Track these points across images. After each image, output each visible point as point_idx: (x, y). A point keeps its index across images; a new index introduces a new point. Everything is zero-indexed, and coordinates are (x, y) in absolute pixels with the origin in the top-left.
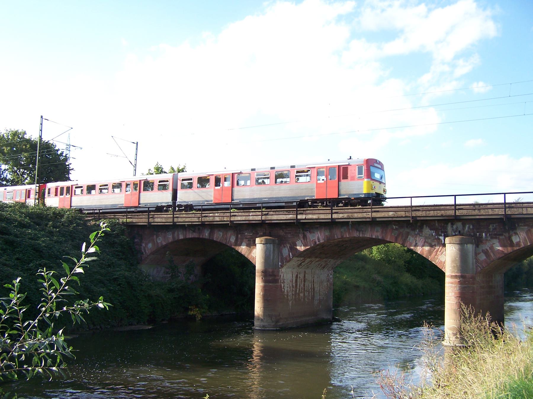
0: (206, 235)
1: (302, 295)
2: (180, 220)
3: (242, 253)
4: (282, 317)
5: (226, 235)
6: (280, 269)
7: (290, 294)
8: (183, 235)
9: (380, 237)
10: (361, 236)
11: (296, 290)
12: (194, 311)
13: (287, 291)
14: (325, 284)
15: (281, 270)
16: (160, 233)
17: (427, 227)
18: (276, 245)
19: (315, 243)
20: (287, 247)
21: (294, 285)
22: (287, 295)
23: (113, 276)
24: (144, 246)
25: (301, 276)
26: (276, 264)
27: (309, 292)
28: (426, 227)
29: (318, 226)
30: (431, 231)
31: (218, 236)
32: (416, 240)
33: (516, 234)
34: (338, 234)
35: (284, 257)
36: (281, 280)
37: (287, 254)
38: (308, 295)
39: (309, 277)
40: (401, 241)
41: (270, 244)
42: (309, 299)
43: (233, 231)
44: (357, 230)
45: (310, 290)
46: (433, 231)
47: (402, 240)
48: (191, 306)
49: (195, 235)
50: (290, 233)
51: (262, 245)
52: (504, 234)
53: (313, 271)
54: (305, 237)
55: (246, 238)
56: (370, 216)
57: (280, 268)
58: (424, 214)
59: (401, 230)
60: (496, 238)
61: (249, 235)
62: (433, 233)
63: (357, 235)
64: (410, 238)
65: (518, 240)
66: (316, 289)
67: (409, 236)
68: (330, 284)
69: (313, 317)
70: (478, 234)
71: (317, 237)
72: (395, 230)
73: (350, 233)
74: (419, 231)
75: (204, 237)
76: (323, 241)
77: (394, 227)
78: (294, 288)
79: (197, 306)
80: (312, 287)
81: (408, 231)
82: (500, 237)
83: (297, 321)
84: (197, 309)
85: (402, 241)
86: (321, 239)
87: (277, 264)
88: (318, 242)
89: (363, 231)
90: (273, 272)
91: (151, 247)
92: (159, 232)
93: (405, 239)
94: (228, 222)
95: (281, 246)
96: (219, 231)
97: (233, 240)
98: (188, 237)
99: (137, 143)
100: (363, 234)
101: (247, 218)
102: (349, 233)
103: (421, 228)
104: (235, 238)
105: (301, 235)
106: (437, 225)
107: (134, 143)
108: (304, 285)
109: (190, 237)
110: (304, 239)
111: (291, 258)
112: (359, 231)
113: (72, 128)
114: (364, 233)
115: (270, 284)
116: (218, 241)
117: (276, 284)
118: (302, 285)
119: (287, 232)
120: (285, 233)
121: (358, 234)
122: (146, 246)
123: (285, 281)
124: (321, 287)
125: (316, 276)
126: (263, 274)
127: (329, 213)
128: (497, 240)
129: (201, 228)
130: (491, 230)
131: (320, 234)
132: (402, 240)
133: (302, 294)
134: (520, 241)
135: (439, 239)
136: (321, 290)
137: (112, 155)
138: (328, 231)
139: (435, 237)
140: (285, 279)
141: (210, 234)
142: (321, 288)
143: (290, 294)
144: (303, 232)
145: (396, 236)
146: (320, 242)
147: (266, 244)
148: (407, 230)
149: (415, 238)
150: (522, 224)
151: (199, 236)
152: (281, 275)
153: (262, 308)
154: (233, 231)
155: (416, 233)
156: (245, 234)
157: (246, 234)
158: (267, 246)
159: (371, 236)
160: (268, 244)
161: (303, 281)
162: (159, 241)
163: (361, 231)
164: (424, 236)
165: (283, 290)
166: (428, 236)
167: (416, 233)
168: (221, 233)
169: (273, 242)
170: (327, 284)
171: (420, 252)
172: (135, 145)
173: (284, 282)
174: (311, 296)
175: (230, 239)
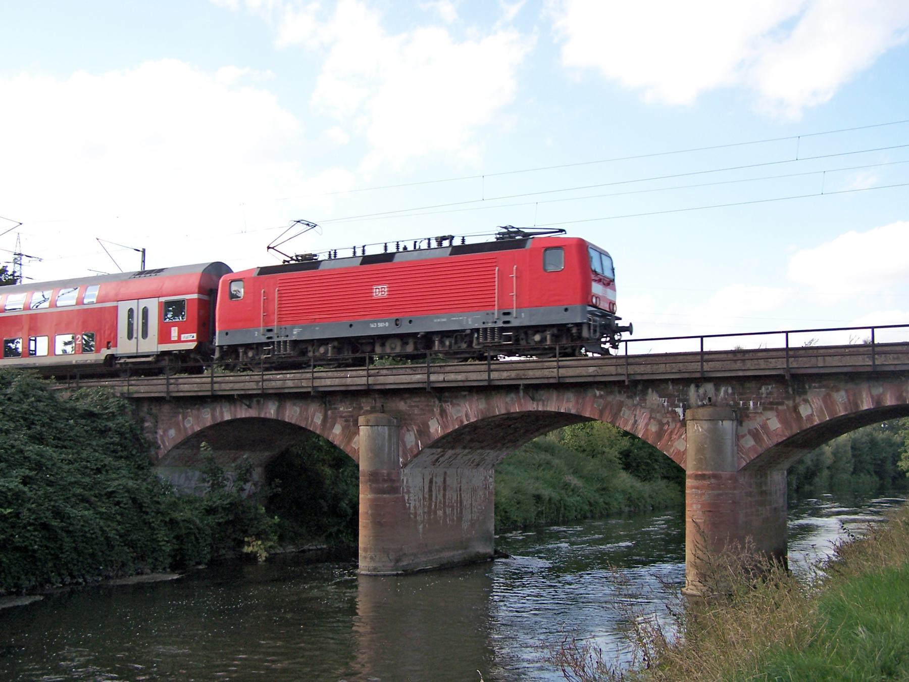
0: (270, 413)
1: (440, 513)
6: (402, 470)
7: (420, 511)
8: (231, 413)
11: (430, 505)
12: (253, 546)
13: (415, 507)
14: (481, 493)
19: (462, 422)
21: (427, 496)
22: (415, 514)
24: (162, 434)
25: (439, 480)
27: (452, 507)
28: (653, 391)
31: (292, 414)
33: (806, 401)
35: (408, 447)
36: (403, 488)
37: (414, 443)
39: (452, 481)
43: (318, 404)
44: (533, 399)
45: (455, 504)
50: (418, 406)
52: (787, 402)
54: (443, 413)
55: (341, 417)
56: (555, 374)
60: (772, 409)
65: (809, 412)
67: (623, 409)
68: (489, 492)
70: (741, 402)
72: (598, 397)
73: (521, 405)
74: (640, 400)
75: (268, 416)
77: (598, 393)
79: (258, 536)
81: (622, 399)
82: (780, 407)
84: (260, 542)
89: (543, 401)
90: (389, 474)
93: (616, 414)
94: (309, 390)
95: (402, 429)
96: (294, 404)
99: (144, 251)
100: (543, 405)
101: (343, 381)
103: (644, 393)
104: (321, 418)
108: (444, 496)
112: (538, 401)
113: (21, 224)
115: (385, 496)
118: (440, 497)
120: (409, 407)
125: (464, 481)
128: (775, 413)
130: (764, 396)
134: (812, 415)
135: (675, 412)
136: (473, 505)
141: (278, 411)
145: (601, 408)
150: (817, 385)
154: (318, 404)
157: (341, 409)
161: (442, 488)
162: (188, 425)
165: (408, 505)
168: (298, 409)
170: (485, 494)
173: (408, 492)
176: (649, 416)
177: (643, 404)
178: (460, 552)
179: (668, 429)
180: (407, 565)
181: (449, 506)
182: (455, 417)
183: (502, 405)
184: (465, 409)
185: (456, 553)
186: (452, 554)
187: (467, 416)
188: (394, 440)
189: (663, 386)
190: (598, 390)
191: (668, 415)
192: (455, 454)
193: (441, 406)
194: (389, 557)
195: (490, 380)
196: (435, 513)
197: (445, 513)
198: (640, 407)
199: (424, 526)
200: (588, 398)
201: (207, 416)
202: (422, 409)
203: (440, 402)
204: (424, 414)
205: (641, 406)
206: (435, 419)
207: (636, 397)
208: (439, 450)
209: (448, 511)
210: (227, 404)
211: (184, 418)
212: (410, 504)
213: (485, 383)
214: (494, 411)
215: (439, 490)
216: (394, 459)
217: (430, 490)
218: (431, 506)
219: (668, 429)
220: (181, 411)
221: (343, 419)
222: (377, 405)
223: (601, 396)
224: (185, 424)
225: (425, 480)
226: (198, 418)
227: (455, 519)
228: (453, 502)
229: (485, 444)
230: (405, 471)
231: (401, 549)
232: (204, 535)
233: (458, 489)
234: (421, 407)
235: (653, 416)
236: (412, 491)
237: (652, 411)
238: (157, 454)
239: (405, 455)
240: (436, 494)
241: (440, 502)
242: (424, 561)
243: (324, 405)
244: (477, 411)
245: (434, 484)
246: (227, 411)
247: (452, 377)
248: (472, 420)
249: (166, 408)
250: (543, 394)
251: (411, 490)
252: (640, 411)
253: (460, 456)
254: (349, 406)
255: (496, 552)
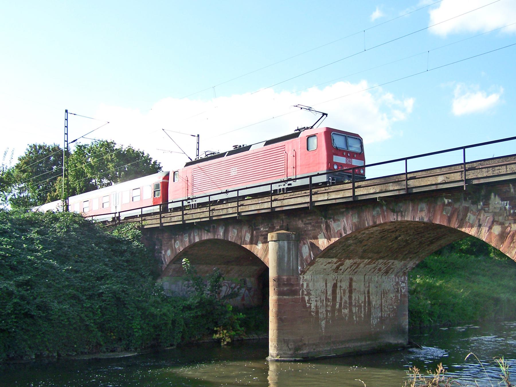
1: (346, 311)
2: (190, 217)
3: (258, 256)
4: (307, 343)
5: (241, 233)
6: (301, 276)
7: (322, 310)
8: (199, 236)
9: (426, 220)
10: (399, 219)
11: (334, 305)
12: (220, 333)
13: (316, 306)
14: (392, 295)
15: (303, 277)
16: (177, 236)
17: (497, 197)
18: (292, 242)
20: (308, 244)
21: (330, 297)
22: (317, 312)
23: (98, 290)
24: (164, 253)
25: (345, 285)
26: (293, 269)
27: (360, 307)
28: (495, 196)
29: (344, 210)
30: (503, 202)
32: (479, 220)
34: (369, 220)
36: (303, 292)
37: (308, 254)
38: (358, 311)
39: (359, 285)
40: (457, 223)
41: (284, 240)
42: (361, 317)
43: (248, 226)
44: (393, 211)
45: (363, 305)
46: (506, 202)
47: (457, 221)
48: (217, 328)
49: (206, 236)
50: (310, 223)
51: (273, 242)
53: (367, 277)
54: (328, 228)
57: (301, 274)
58: (484, 173)
59: (456, 206)
61: (264, 231)
62: (506, 205)
63: (394, 219)
64: (470, 216)
66: (374, 303)
67: (469, 214)
68: (401, 295)
69: (368, 342)
71: (343, 227)
72: (447, 205)
73: (385, 217)
74: (484, 204)
75: (219, 237)
76: (350, 232)
77: (446, 201)
78: (329, 301)
79: (225, 327)
80: (367, 300)
81: (467, 206)
83: (337, 347)
84: (225, 331)
85: (458, 223)
86: (347, 229)
87: (294, 268)
88: (345, 233)
89: (402, 212)
90: (288, 280)
91: (170, 254)
92: (177, 235)
93: (462, 220)
94: (236, 215)
95: (300, 242)
96: (234, 228)
97: (248, 237)
98: (203, 239)
99: (198, 136)
100: (402, 216)
102: (384, 217)
103: (487, 198)
104: (250, 237)
105: (324, 225)
106: (512, 190)
107: (194, 136)
108: (350, 297)
109: (206, 239)
110: (327, 231)
111: (312, 259)
112: (397, 212)
114: (404, 214)
115: (285, 297)
116: (233, 241)
117: (293, 297)
119: (307, 222)
120: (305, 224)
121: (395, 217)
122: (165, 254)
123: (311, 292)
124: (383, 301)
125: (372, 285)
126: (275, 283)
127: (350, 188)
129: (216, 226)
131: (347, 222)
132: (457, 221)
133: (346, 310)
136: (383, 305)
137: (164, 151)
138: (357, 217)
139: (510, 211)
140: (311, 289)
142: (383, 302)
143: (322, 310)
144: (326, 220)
145: (449, 215)
146: (346, 233)
147: (278, 241)
148: (465, 204)
149: (478, 216)
151: (214, 236)
152: (303, 284)
153: (275, 331)
154: (248, 226)
155: (479, 207)
156: (260, 229)
157: (262, 229)
158: (279, 243)
159: (413, 219)
160: (281, 241)
161: (347, 291)
162: (177, 247)
163: (399, 212)
164: (492, 212)
165: (308, 305)
166: (498, 211)
167: (479, 207)
169: (287, 238)
170: (396, 297)
171: (486, 239)
172: (196, 138)
173: (309, 294)
174: (365, 312)
175: (244, 238)
176: (491, 220)
177: (487, 209)
178: (368, 342)
179: (510, 231)
180: (308, 353)
181: (355, 306)
182: (336, 231)
183: (370, 218)
184: (343, 224)
185: (364, 343)
186: (359, 344)
187: (345, 229)
188: (293, 252)
189: (505, 189)
190: (446, 199)
191: (510, 218)
192: (355, 263)
193: (326, 222)
194: (288, 346)
195: (354, 196)
196: (340, 310)
197: (351, 310)
198: (483, 211)
199: (327, 322)
200: (438, 206)
201: (186, 240)
202: (313, 226)
203: (325, 219)
204: (315, 230)
205: (484, 210)
206: (322, 233)
207: (480, 202)
208: (335, 260)
209: (354, 310)
210: (197, 231)
211: (175, 241)
212: (311, 304)
213: (351, 199)
214: (364, 224)
215: (344, 293)
216: (293, 267)
217: (334, 292)
218: (336, 305)
219: (510, 231)
220: (173, 236)
221: (263, 237)
222: (284, 224)
223: (449, 204)
224: (176, 246)
225: (329, 284)
226: (182, 241)
227: (363, 316)
228: (361, 302)
229: (381, 255)
230: (305, 276)
231: (301, 340)
232: (178, 325)
233: (366, 293)
234: (312, 224)
235: (496, 219)
236: (313, 294)
237: (495, 214)
238: (162, 267)
239: (302, 265)
240: (341, 296)
241: (346, 302)
242: (324, 350)
243: (251, 227)
244: (352, 225)
245: (338, 288)
246: (197, 235)
247: (333, 196)
248: (348, 233)
249: (166, 235)
250: (401, 206)
251: (312, 293)
252: (484, 215)
253: (362, 265)
254: (267, 227)
255: (410, 343)
